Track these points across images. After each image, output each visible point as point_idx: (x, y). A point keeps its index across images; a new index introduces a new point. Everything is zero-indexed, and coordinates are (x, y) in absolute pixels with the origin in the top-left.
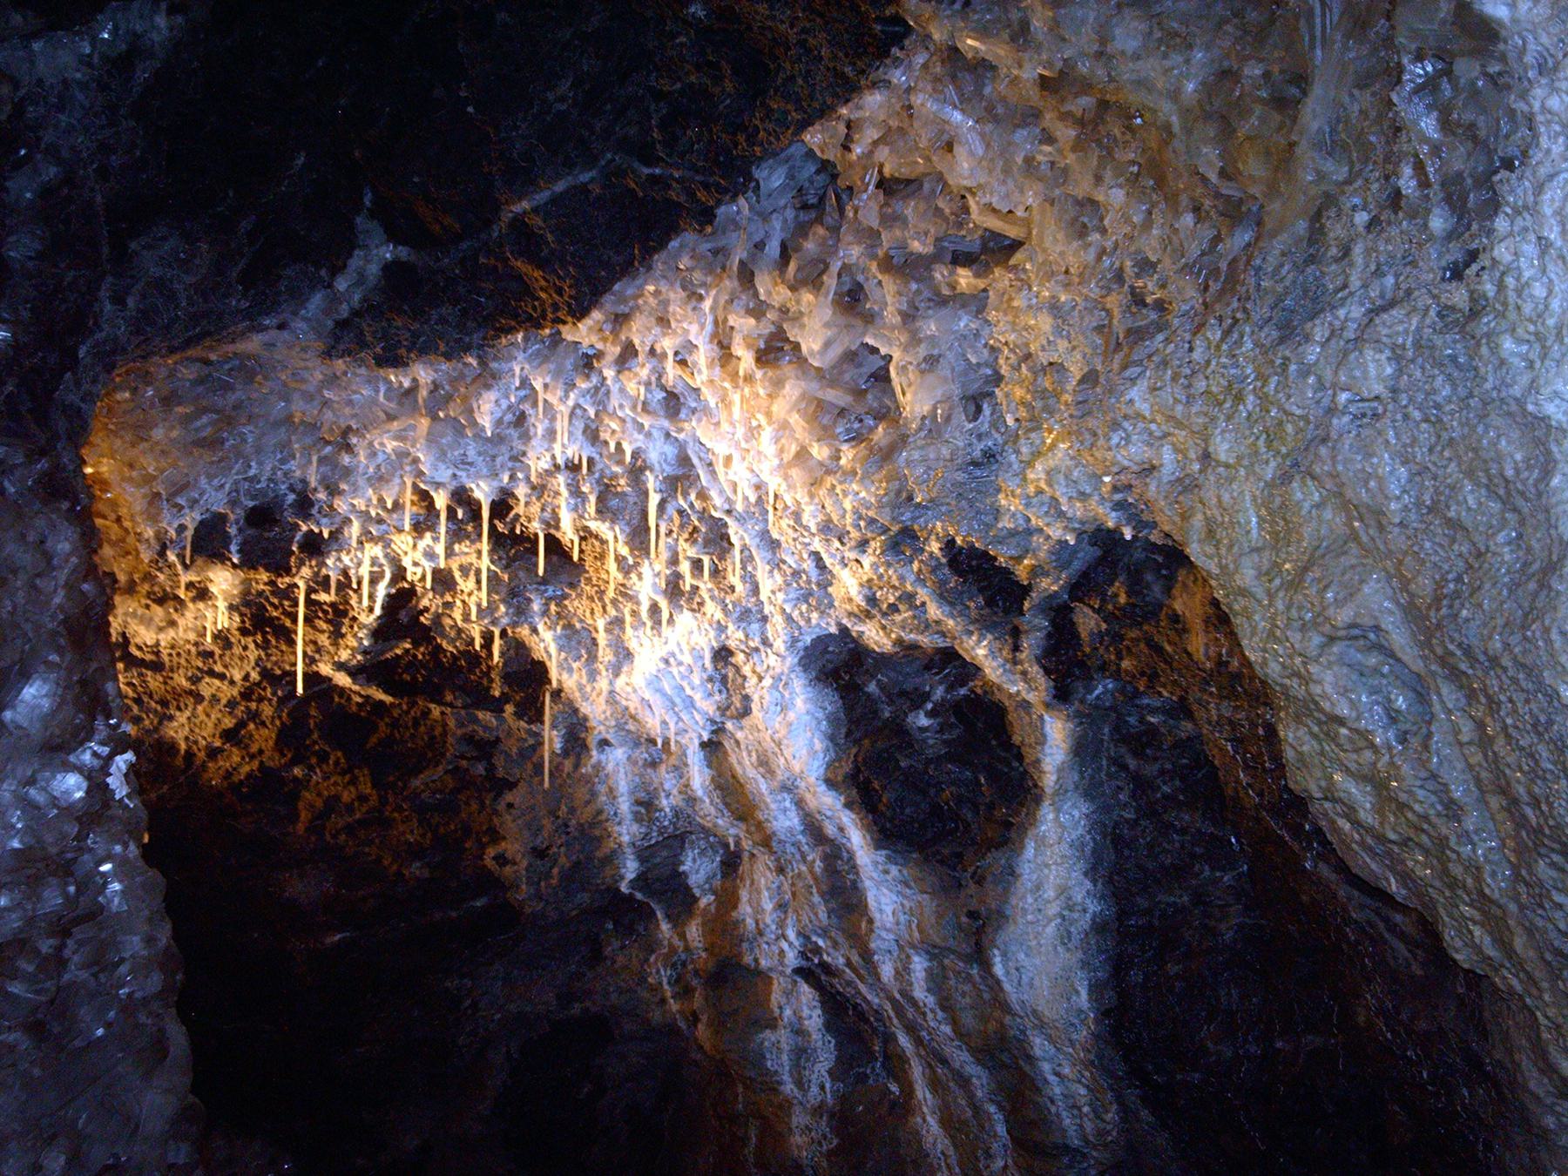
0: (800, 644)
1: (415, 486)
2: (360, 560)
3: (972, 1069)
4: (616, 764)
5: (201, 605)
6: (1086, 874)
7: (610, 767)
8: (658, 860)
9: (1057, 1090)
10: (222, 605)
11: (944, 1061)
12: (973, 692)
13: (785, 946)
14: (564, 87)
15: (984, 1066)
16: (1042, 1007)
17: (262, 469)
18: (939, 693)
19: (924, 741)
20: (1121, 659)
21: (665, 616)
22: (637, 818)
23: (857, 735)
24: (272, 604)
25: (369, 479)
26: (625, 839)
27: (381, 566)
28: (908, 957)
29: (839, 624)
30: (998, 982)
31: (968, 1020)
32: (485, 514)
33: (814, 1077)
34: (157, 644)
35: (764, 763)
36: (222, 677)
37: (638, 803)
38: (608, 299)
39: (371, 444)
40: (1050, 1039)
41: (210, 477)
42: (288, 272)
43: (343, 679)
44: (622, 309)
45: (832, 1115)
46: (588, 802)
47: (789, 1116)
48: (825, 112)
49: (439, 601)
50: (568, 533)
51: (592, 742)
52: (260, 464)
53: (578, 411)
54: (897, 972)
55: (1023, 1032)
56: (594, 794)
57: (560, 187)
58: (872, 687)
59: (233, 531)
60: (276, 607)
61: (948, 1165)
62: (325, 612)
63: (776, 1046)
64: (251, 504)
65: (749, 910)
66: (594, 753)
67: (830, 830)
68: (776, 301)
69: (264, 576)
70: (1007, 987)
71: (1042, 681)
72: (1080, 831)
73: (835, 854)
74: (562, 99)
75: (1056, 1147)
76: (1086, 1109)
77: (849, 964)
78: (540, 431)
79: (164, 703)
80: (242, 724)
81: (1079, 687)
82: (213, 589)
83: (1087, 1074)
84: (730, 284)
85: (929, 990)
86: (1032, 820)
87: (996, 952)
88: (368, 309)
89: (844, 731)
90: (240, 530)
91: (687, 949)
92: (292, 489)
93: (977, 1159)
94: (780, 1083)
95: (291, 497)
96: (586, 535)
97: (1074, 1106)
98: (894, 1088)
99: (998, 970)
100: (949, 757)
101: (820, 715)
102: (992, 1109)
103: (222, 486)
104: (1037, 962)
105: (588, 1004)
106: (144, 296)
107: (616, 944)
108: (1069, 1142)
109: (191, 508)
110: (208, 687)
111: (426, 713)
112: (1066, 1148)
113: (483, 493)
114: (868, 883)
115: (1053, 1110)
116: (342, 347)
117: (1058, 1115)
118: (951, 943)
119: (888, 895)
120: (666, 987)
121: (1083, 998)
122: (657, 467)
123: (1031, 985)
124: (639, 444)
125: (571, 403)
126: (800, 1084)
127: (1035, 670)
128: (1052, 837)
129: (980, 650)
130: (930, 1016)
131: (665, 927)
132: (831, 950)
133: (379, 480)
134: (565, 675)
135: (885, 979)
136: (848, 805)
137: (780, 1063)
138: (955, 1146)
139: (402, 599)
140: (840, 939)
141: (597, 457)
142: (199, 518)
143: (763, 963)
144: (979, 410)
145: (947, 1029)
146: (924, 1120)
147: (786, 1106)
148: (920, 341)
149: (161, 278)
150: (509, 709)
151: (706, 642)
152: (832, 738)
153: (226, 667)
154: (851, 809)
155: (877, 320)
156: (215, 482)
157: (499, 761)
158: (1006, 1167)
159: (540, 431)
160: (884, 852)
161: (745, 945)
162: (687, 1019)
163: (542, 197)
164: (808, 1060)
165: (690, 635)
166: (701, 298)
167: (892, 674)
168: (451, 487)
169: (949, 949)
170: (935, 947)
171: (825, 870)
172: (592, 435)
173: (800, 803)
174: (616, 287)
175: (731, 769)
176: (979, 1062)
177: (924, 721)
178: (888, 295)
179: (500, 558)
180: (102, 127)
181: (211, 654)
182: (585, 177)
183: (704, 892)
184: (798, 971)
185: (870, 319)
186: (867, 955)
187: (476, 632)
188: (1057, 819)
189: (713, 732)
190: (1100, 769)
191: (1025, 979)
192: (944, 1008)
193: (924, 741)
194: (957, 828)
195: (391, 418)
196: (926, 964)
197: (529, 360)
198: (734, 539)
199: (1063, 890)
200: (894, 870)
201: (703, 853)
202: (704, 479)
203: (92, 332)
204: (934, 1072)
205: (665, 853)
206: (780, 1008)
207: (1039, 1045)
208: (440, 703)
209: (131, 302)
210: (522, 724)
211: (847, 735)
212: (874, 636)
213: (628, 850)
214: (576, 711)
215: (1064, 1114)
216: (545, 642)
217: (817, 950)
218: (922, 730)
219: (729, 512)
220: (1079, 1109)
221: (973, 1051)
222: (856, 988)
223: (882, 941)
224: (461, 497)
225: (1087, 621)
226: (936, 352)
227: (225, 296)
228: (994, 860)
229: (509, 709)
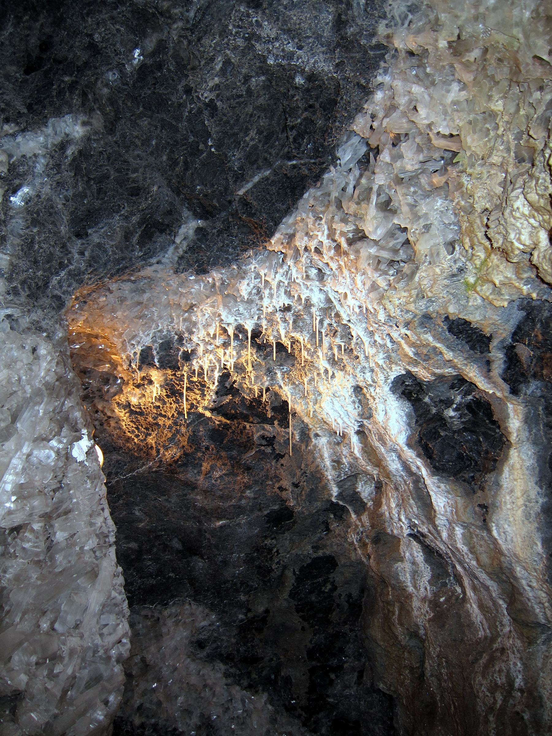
0: (389, 381)
1: (220, 326)
2: (203, 361)
3: (489, 583)
4: (323, 442)
5: (151, 387)
6: (536, 483)
7: (320, 446)
8: (347, 487)
9: (531, 594)
10: (157, 385)
11: (476, 578)
12: (475, 397)
13: (401, 523)
14: (253, 133)
15: (495, 581)
16: (518, 551)
17: (163, 325)
18: (458, 399)
19: (452, 423)
20: (542, 369)
21: (330, 373)
22: (334, 468)
23: (420, 422)
24: (176, 384)
25: (204, 326)
26: (330, 477)
27: (214, 363)
28: (454, 528)
29: (405, 369)
30: (496, 539)
31: (485, 559)
32: (249, 335)
33: (422, 584)
34: (140, 404)
35: (382, 439)
36: (165, 416)
37: (333, 461)
38: (282, 226)
39: (201, 310)
40: (525, 569)
41: (144, 332)
42: (160, 239)
43: (208, 414)
44: (290, 231)
45: (430, 602)
46: (313, 462)
47: (411, 602)
48: (359, 109)
49: (239, 377)
50: (286, 342)
51: (312, 436)
52: (162, 324)
53: (281, 284)
54: (449, 535)
55: (511, 564)
56: (315, 459)
57: (256, 179)
58: (427, 400)
59: (155, 353)
60: (178, 385)
61: (483, 628)
62: (197, 386)
63: (404, 572)
64: (161, 341)
65: (386, 508)
66: (313, 440)
67: (414, 469)
68: (351, 211)
69: (169, 372)
70: (500, 542)
71: (506, 387)
72: (532, 461)
73: (417, 480)
74: (252, 139)
75: (533, 623)
76: (547, 604)
77: (430, 531)
78: (266, 295)
79: (147, 429)
80: (174, 435)
81: (523, 387)
82: (153, 379)
83: (545, 586)
84: (333, 208)
85: (464, 544)
86: (507, 457)
87: (493, 524)
88: (191, 249)
89: (414, 421)
90: (158, 353)
91: (363, 526)
92: (176, 334)
93: (497, 626)
94: (407, 587)
95: (176, 337)
96: (294, 342)
97: (540, 603)
98: (459, 590)
99: (495, 533)
100: (465, 429)
101: (403, 414)
102: (501, 602)
103: (148, 335)
104: (514, 529)
105: (325, 550)
106: (93, 251)
107: (336, 525)
108: (539, 621)
109: (138, 345)
110: (161, 421)
111: (245, 427)
112: (539, 624)
113: (249, 326)
114: (431, 493)
115: (530, 604)
116: (181, 267)
117: (532, 607)
118: (471, 520)
119: (442, 497)
120: (356, 543)
121: (539, 547)
122: (317, 304)
123: (512, 541)
124: (308, 295)
125: (277, 280)
126: (415, 587)
127: (500, 381)
128: (518, 466)
129: (473, 373)
130: (466, 556)
131: (353, 516)
132: (421, 526)
133: (207, 325)
134: (296, 405)
135: (444, 539)
136: (419, 456)
137: (407, 579)
138: (486, 619)
139: (225, 376)
140: (425, 521)
141: (292, 304)
142: (141, 348)
143: (395, 532)
144: (454, 248)
145: (474, 563)
146: (471, 606)
147: (409, 597)
148: (419, 218)
149: (99, 243)
150: (276, 422)
151: (350, 383)
152: (409, 425)
153: (165, 412)
154: (420, 458)
155: (399, 212)
156: (146, 333)
157: (276, 446)
158: (510, 631)
159: (266, 295)
160: (436, 477)
161: (387, 524)
162: (365, 557)
163: (249, 185)
164: (418, 576)
165: (343, 384)
166: (321, 219)
167: (436, 393)
168: (234, 325)
169: (471, 523)
170: (464, 522)
171: (414, 488)
172: (288, 294)
173: (399, 457)
174: (284, 220)
175: (370, 443)
176: (491, 579)
177: (452, 413)
178: (402, 198)
179: (261, 356)
180: (56, 174)
181: (159, 407)
182: (268, 173)
183: (369, 500)
184: (410, 535)
185: (394, 212)
186: (435, 527)
187: (256, 388)
188: (519, 456)
189: (359, 426)
190: (539, 430)
191: (509, 538)
192: (471, 553)
193: (452, 423)
194: (471, 464)
195: (208, 297)
196: (462, 531)
197: (258, 263)
198: (353, 334)
199: (525, 492)
200: (442, 485)
201: (366, 483)
202: (338, 307)
203: (68, 266)
204: (474, 583)
205: (349, 484)
206: (404, 552)
207: (519, 571)
208: (248, 422)
209: (87, 254)
210: (283, 429)
211: (417, 421)
212: (423, 373)
213: (332, 482)
214: (303, 421)
215: (536, 606)
216: (287, 392)
217: (415, 525)
218: (451, 417)
219: (349, 321)
220: (543, 604)
221: (488, 574)
222: (435, 543)
223: (441, 521)
224: (240, 329)
225: (524, 352)
226: (429, 222)
227: (133, 251)
228: (490, 477)
229: (276, 422)
